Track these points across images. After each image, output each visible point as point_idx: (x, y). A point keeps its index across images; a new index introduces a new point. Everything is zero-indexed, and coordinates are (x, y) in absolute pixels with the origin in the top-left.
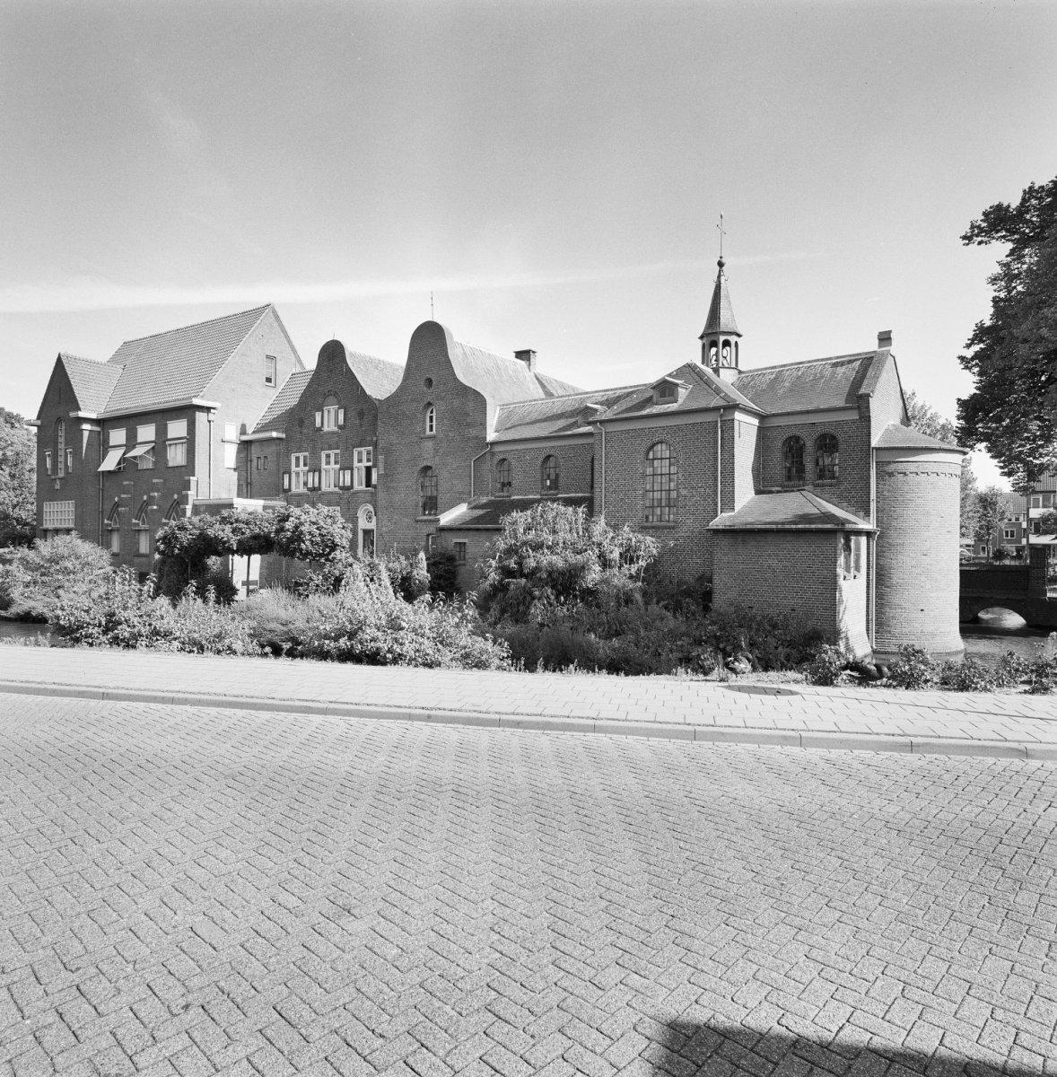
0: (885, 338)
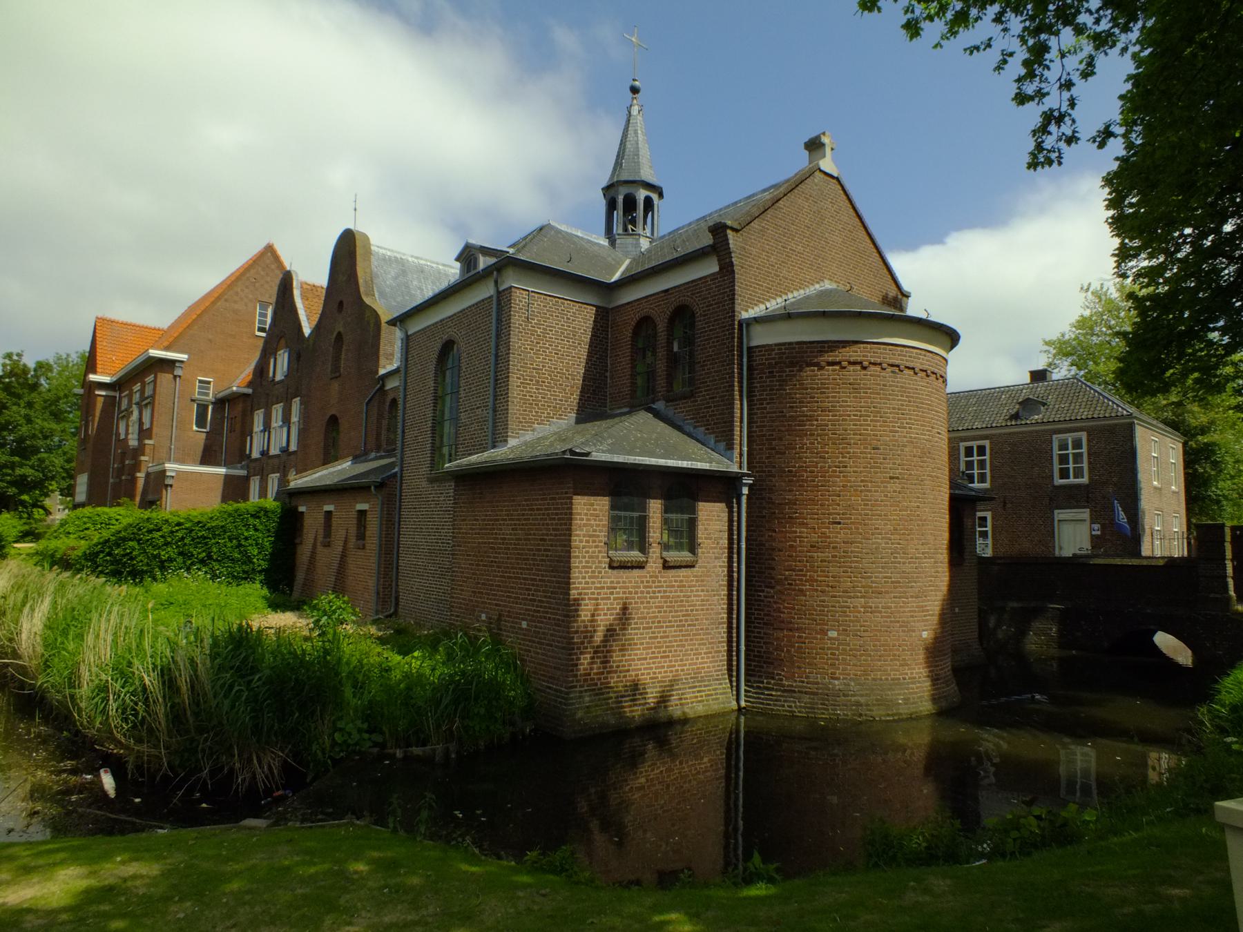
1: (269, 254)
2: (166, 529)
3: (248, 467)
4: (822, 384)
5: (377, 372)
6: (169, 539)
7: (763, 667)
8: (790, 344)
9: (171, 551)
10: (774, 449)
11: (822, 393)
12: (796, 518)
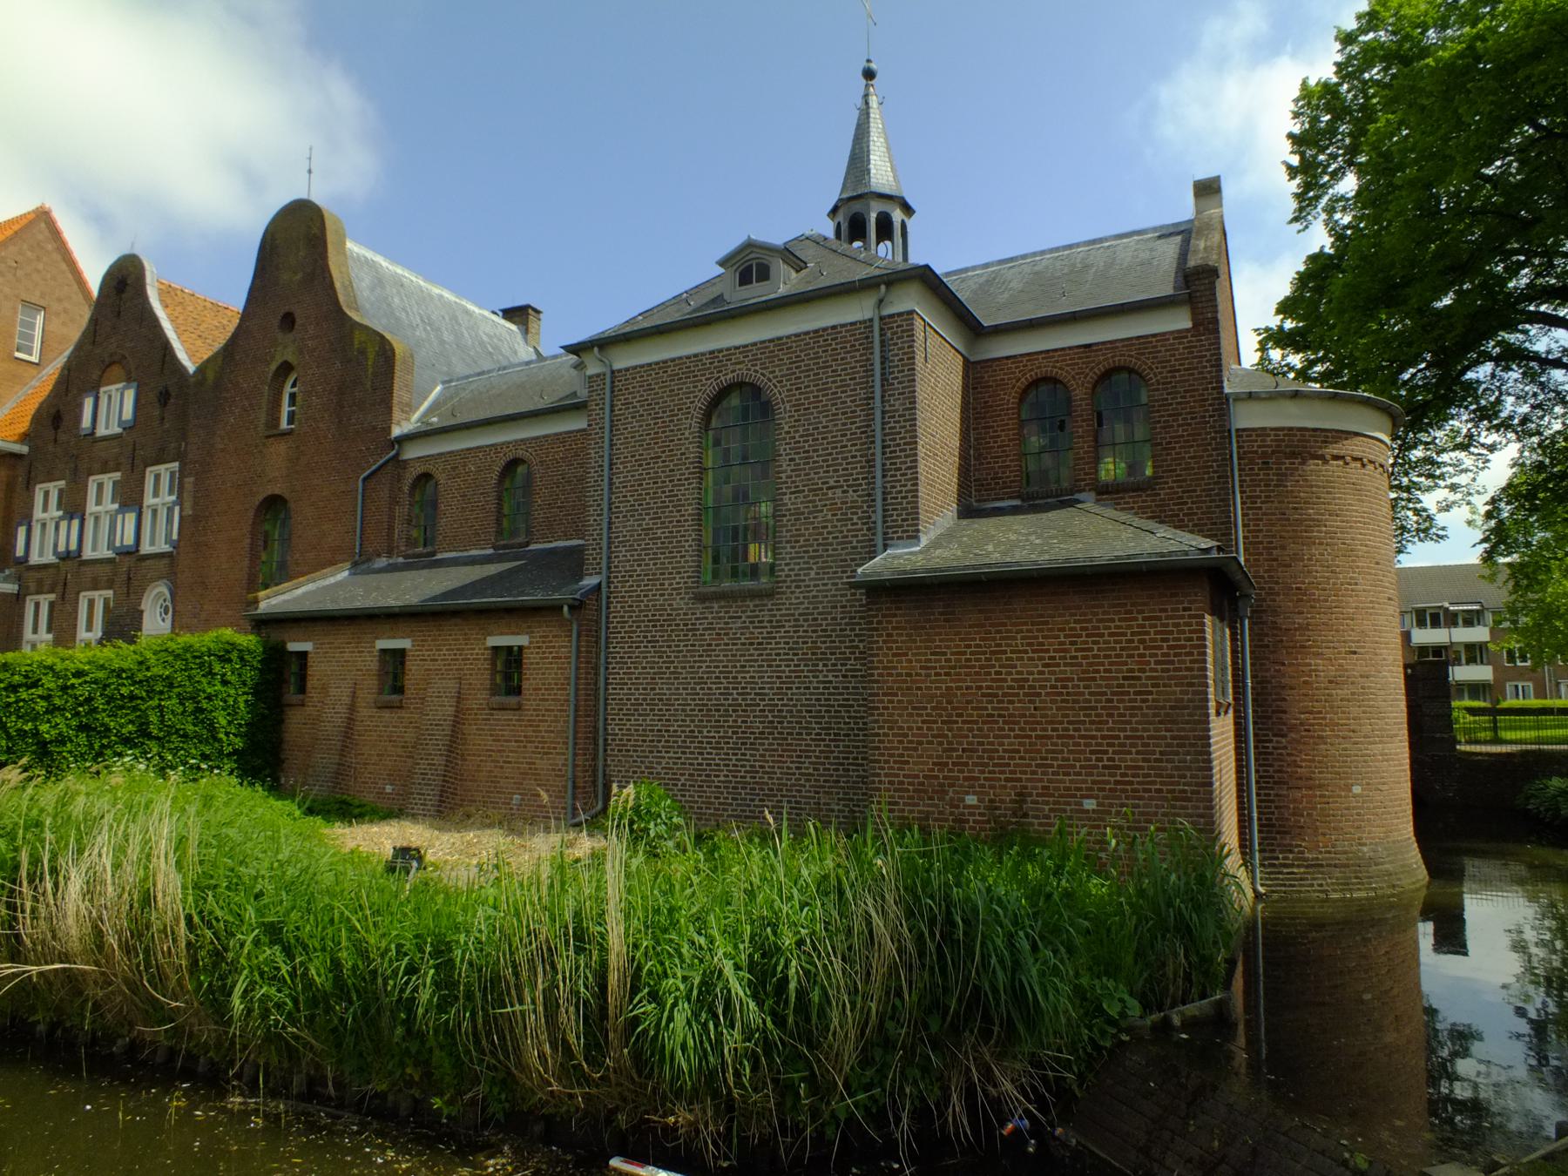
0: (1208, 190)
1: (43, 225)
2: (49, 682)
3: (19, 579)
4: (1327, 481)
5: (388, 430)
6: (57, 702)
7: (1275, 839)
8: (1291, 429)
9: (63, 724)
10: (1276, 560)
11: (1328, 493)
12: (1310, 647)
